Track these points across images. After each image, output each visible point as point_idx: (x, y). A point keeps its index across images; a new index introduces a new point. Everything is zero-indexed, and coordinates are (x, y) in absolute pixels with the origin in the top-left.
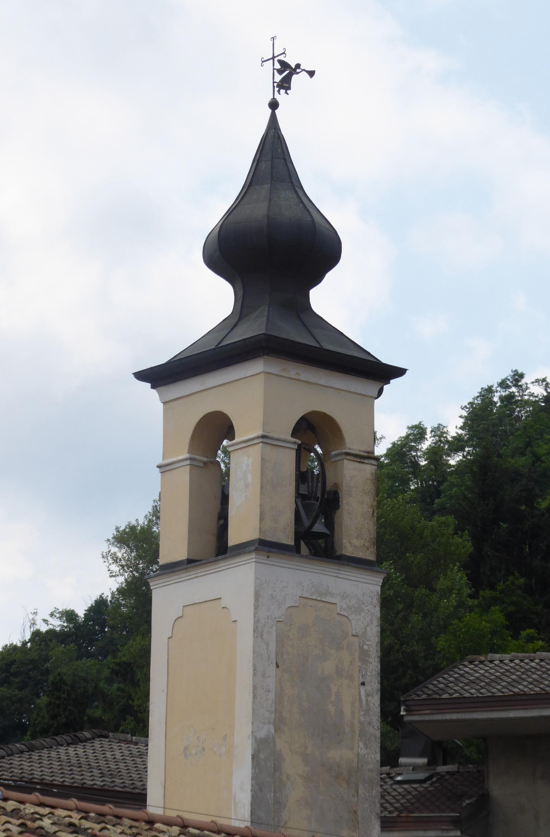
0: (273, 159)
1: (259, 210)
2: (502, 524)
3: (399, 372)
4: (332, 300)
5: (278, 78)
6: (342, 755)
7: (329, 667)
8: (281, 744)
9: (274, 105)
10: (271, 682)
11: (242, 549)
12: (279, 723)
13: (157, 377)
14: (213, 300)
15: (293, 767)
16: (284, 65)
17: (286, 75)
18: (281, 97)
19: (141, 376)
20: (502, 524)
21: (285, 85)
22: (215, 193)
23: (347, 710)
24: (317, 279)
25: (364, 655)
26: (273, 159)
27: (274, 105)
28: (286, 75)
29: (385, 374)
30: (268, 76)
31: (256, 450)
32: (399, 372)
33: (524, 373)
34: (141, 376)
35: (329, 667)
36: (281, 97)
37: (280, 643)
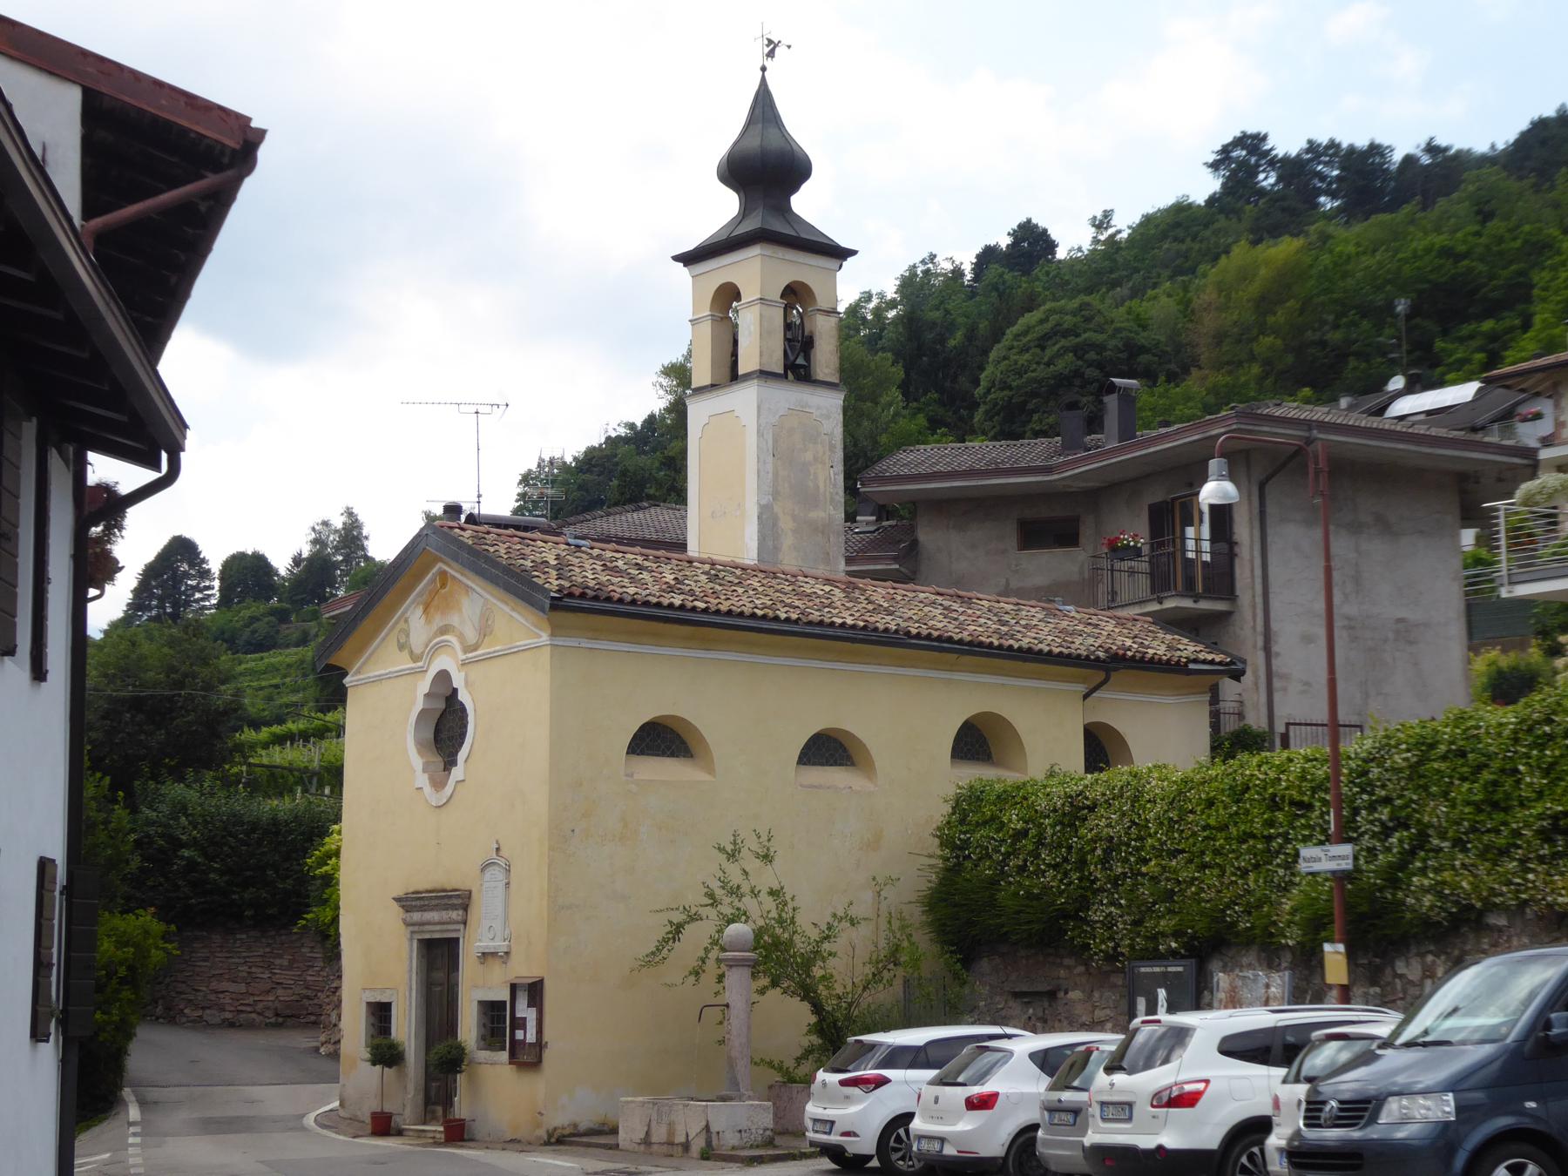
0: (764, 108)
3: (853, 253)
4: (804, 203)
5: (767, 50)
6: (817, 515)
7: (809, 456)
8: (777, 509)
9: (764, 69)
10: (770, 467)
12: (776, 494)
13: (688, 259)
14: (723, 206)
16: (770, 42)
17: (772, 48)
18: (769, 63)
19: (677, 258)
21: (771, 54)
22: (725, 129)
23: (821, 485)
24: (795, 188)
25: (832, 448)
26: (764, 108)
27: (764, 69)
28: (772, 48)
30: (760, 49)
31: (756, 309)
32: (853, 253)
34: (677, 258)
35: (809, 456)
36: (769, 63)
37: (775, 441)
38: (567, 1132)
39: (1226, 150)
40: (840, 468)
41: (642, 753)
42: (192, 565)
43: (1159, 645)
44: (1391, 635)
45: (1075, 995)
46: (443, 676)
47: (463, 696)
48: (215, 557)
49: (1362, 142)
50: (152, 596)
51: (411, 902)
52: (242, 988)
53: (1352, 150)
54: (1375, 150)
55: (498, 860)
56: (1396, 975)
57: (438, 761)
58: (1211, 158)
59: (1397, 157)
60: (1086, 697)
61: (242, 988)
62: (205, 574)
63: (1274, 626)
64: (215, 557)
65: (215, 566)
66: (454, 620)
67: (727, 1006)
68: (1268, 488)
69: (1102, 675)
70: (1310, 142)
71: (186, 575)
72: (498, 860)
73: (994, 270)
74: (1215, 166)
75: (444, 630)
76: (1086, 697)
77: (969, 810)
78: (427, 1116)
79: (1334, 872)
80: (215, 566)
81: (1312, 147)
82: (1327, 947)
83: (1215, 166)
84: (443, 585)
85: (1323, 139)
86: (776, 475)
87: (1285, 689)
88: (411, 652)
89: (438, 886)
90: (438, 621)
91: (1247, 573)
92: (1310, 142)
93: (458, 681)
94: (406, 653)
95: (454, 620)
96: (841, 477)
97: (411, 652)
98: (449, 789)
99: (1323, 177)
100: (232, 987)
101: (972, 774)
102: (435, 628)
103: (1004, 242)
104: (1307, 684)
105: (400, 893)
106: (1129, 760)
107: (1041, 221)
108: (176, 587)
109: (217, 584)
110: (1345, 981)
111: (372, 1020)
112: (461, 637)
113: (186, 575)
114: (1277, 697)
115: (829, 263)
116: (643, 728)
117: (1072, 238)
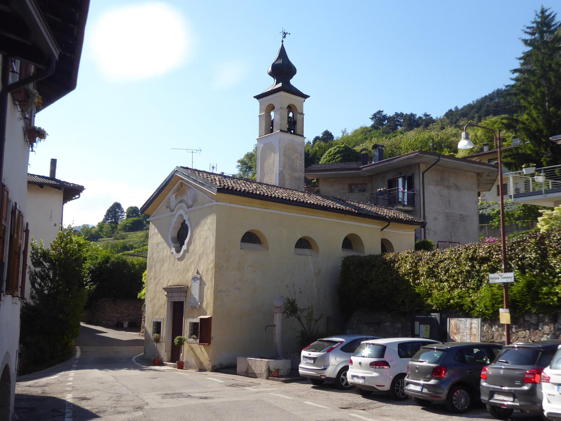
0: (283, 53)
1: (280, 61)
2: (71, 25)
3: (308, 97)
4: (294, 82)
6: (296, 175)
7: (294, 157)
8: (284, 172)
9: (283, 41)
10: (283, 159)
11: (304, 379)
12: (284, 168)
13: (258, 97)
14: (270, 83)
15: (287, 177)
16: (284, 33)
17: (285, 34)
19: (255, 97)
20: (71, 25)
21: (285, 37)
23: (298, 165)
24: (291, 78)
25: (301, 155)
26: (283, 53)
27: (283, 41)
28: (285, 34)
29: (306, 97)
30: (281, 35)
32: (308, 97)
33: (47, 137)
34: (255, 97)
35: (294, 157)
37: (284, 151)
38: (218, 367)
39: (375, 115)
40: (303, 161)
41: (246, 242)
42: (119, 209)
43: (402, 216)
44: (458, 219)
45: (387, 324)
46: (181, 216)
47: (187, 222)
48: (125, 207)
49: (409, 113)
50: (109, 217)
51: (170, 290)
52: (119, 315)
53: (407, 115)
54: (412, 115)
55: (198, 278)
56: (525, 321)
57: (179, 245)
58: (371, 117)
59: (417, 117)
60: (382, 230)
61: (119, 315)
62: (123, 212)
63: (426, 215)
64: (125, 207)
65: (125, 211)
66: (185, 198)
67: (275, 326)
68: (425, 174)
69: (387, 223)
70: (396, 113)
71: (118, 212)
72: (198, 278)
73: (318, 141)
74: (372, 119)
75: (181, 202)
76: (382, 230)
77: (347, 263)
78: (172, 360)
79: (504, 283)
80: (125, 211)
81: (397, 114)
82: (501, 310)
83: (372, 119)
84: (181, 187)
85: (399, 112)
86: (284, 162)
87: (429, 233)
88: (170, 209)
89: (177, 284)
90: (179, 199)
91: (419, 199)
92: (396, 113)
93: (186, 218)
94: (169, 209)
95: (185, 198)
96: (304, 164)
97: (170, 209)
98: (182, 253)
99: (398, 121)
100: (116, 315)
101: (349, 253)
102: (178, 200)
103: (321, 136)
104: (435, 232)
105: (165, 286)
106: (393, 251)
107: (330, 131)
108: (115, 214)
109: (126, 214)
110: (509, 323)
111: (155, 327)
112: (187, 204)
113: (118, 212)
114: (427, 235)
115: (302, 99)
116: (246, 233)
117: (337, 135)
